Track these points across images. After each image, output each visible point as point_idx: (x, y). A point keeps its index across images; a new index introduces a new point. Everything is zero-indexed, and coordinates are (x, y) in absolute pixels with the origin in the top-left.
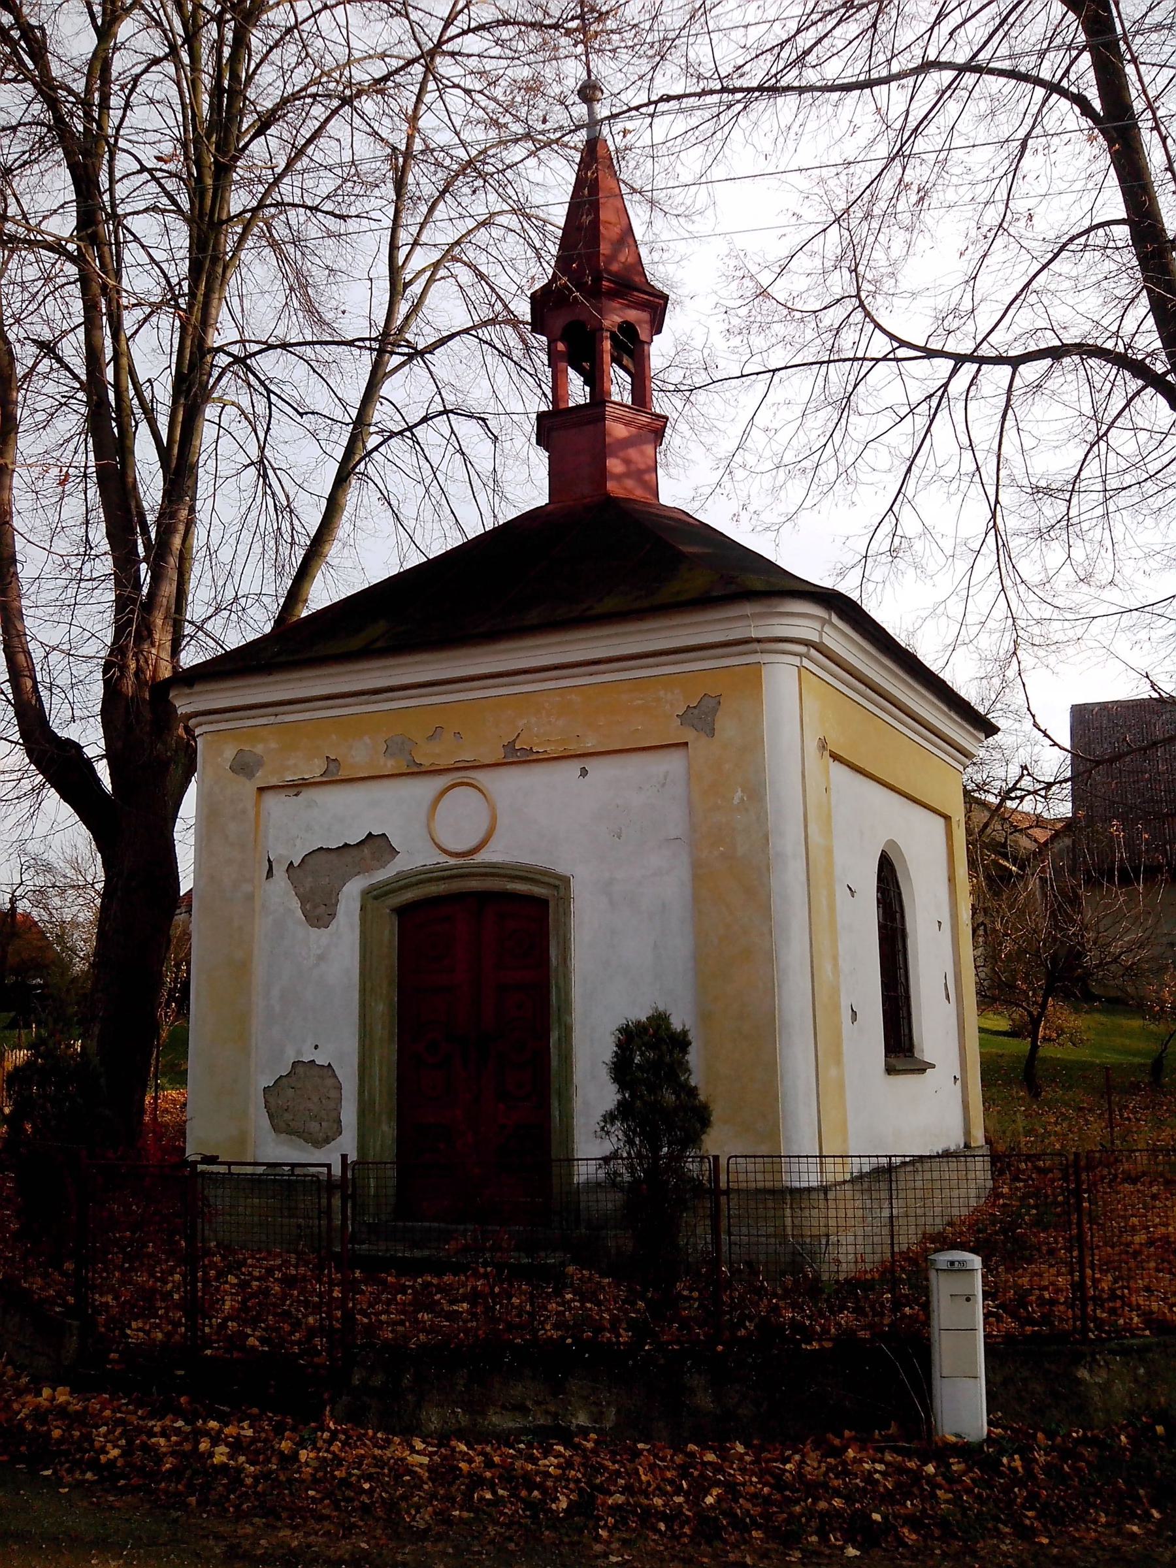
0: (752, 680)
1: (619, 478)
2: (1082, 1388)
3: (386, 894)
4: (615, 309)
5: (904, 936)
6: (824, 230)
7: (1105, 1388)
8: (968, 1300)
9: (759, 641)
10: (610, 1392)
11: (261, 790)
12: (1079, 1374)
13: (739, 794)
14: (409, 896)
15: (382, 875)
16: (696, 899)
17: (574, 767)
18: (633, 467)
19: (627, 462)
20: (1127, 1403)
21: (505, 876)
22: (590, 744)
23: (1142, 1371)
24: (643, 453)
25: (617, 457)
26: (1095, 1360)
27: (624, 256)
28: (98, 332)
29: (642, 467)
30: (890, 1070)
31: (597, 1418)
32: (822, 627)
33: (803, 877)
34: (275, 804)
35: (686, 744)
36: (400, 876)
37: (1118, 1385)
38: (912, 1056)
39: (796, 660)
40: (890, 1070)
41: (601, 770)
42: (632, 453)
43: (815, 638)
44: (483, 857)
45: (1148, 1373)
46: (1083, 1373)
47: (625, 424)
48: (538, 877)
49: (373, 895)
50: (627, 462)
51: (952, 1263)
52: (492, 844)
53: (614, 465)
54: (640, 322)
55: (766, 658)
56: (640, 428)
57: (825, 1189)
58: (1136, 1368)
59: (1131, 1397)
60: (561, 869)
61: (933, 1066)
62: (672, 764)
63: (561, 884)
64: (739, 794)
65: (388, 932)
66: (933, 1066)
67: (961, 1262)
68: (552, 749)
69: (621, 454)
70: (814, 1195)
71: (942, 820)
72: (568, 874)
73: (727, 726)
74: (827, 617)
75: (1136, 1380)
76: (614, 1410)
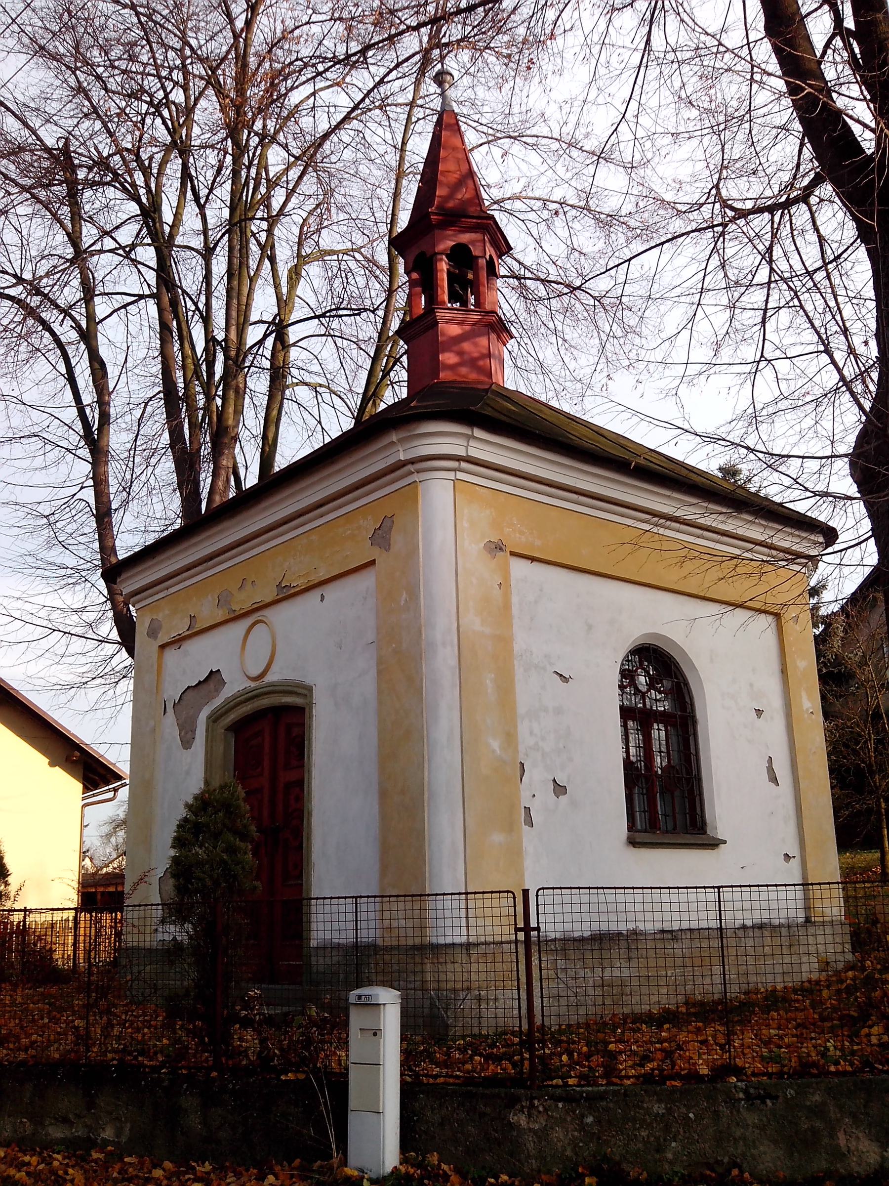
0: (410, 496)
1: (452, 367)
2: (515, 1134)
3: (221, 716)
4: (449, 236)
5: (694, 722)
6: (616, 130)
7: (542, 1135)
8: (375, 1034)
9: (412, 462)
10: (127, 1109)
11: (163, 647)
12: (513, 1119)
13: (404, 595)
14: (232, 717)
15: (218, 702)
16: (380, 692)
17: (315, 595)
18: (466, 357)
19: (460, 353)
20: (569, 1153)
21: (281, 692)
22: (323, 575)
23: (590, 1120)
24: (476, 345)
25: (451, 351)
26: (532, 1105)
27: (464, 194)
28: (170, 345)
29: (476, 355)
30: (633, 842)
31: (119, 1133)
32: (468, 442)
33: (454, 662)
34: (171, 655)
35: (372, 563)
36: (227, 701)
37: (558, 1133)
38: (705, 833)
39: (451, 475)
40: (633, 842)
41: (333, 592)
42: (466, 346)
43: (461, 452)
44: (270, 678)
45: (598, 1121)
46: (522, 1120)
47: (458, 324)
48: (295, 689)
49: (214, 718)
50: (460, 353)
51: (360, 997)
52: (275, 667)
53: (448, 358)
54: (473, 242)
55: (416, 477)
56: (473, 325)
57: (468, 945)
58: (583, 1116)
59: (576, 1146)
60: (308, 681)
61: (725, 842)
62: (365, 582)
63: (305, 691)
64: (404, 595)
65: (226, 748)
66: (725, 842)
67: (369, 997)
68: (301, 583)
69: (455, 348)
70: (458, 950)
71: (770, 618)
72: (312, 684)
73: (397, 540)
74: (470, 433)
75: (582, 1127)
76: (129, 1125)
